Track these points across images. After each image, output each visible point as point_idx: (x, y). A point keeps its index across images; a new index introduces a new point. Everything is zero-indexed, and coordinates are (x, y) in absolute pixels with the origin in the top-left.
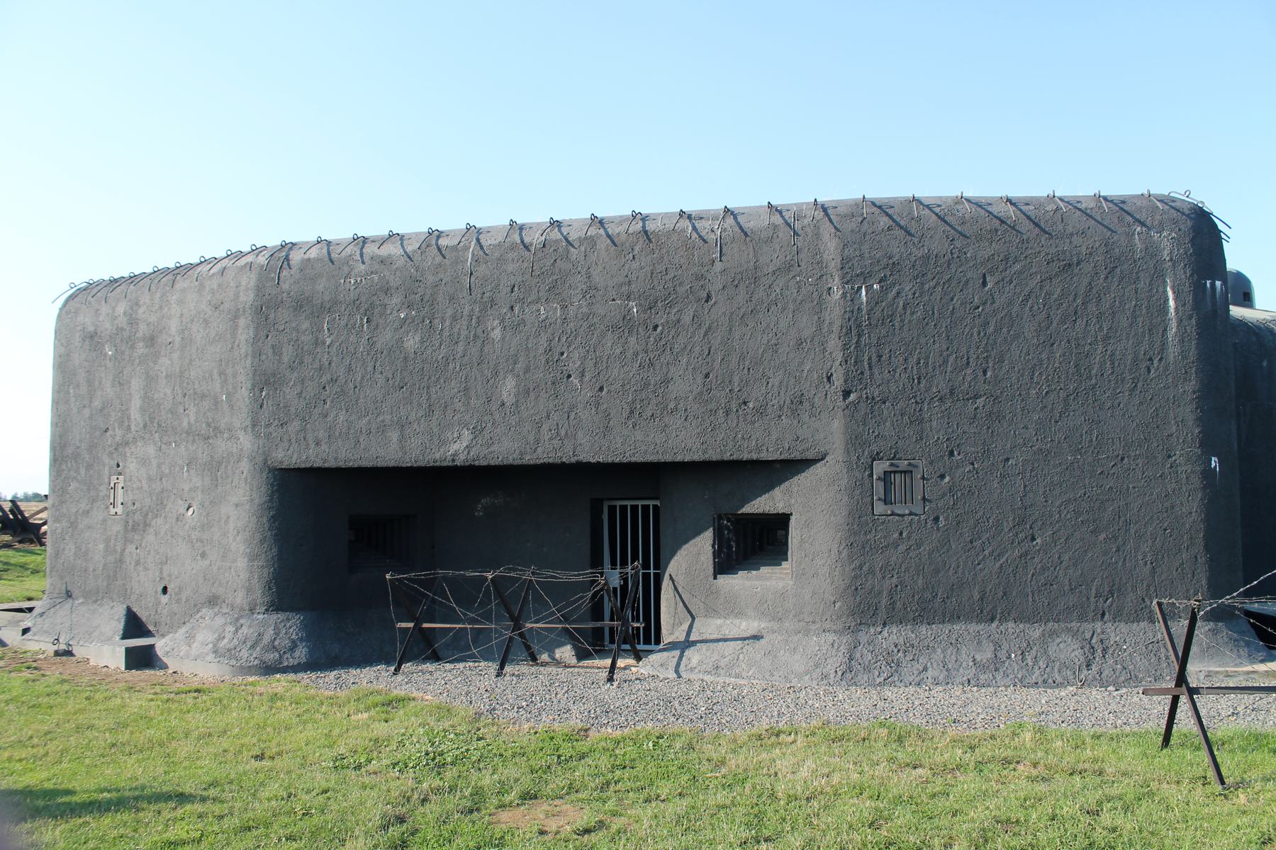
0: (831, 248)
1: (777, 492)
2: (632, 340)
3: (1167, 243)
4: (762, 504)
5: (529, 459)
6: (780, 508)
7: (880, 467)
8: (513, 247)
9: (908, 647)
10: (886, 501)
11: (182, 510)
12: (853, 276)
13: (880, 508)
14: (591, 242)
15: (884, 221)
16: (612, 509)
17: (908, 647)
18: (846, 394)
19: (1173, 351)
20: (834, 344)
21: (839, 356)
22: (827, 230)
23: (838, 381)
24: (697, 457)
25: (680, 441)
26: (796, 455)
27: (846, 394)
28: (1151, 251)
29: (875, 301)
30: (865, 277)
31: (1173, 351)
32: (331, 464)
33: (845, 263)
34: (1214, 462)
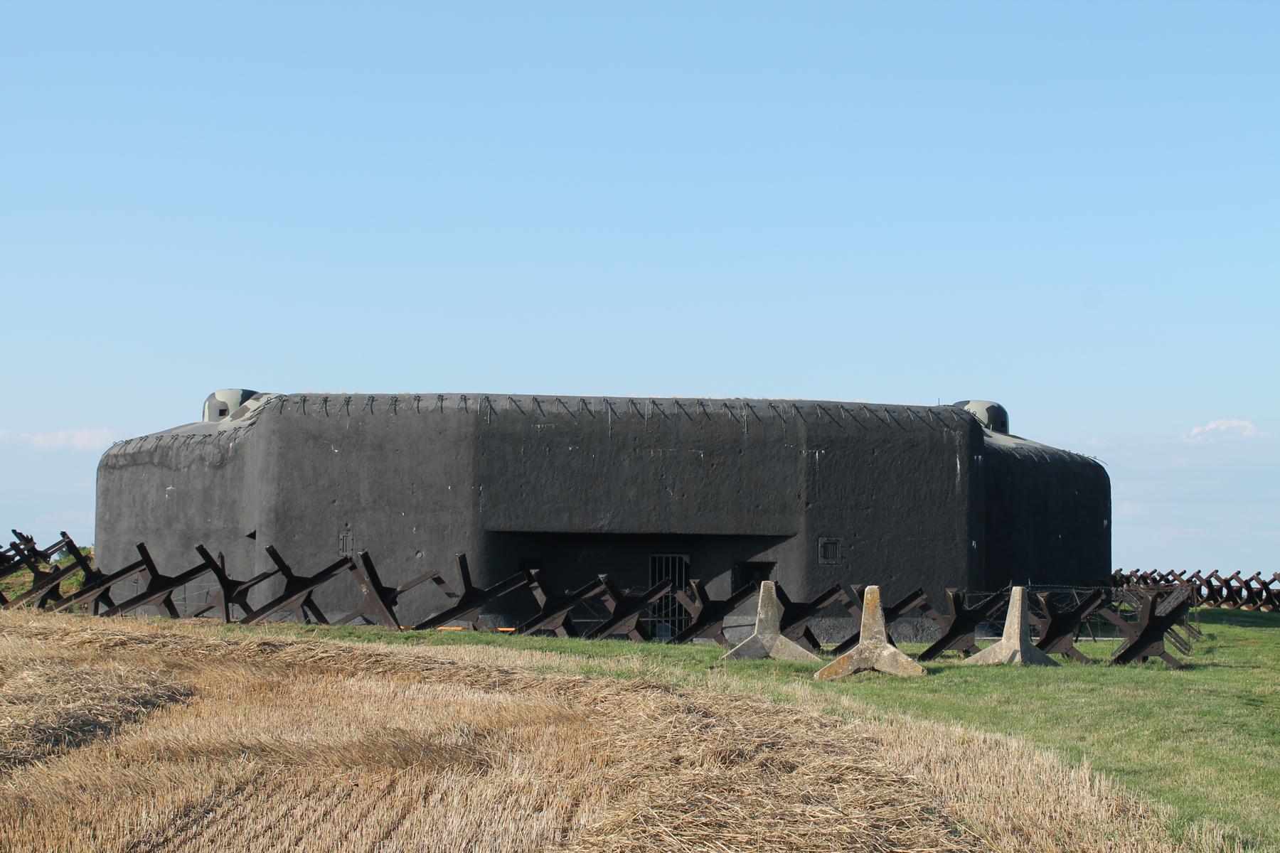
0: (802, 432)
1: (770, 551)
2: (701, 471)
3: (958, 436)
4: (760, 557)
5: (644, 530)
6: (771, 559)
7: (821, 541)
8: (633, 416)
9: (835, 627)
10: (825, 557)
11: (412, 554)
12: (812, 444)
13: (821, 561)
14: (678, 416)
15: (827, 419)
16: (654, 559)
17: (835, 627)
18: (807, 504)
19: (958, 489)
20: (802, 479)
21: (805, 485)
22: (800, 421)
23: (804, 498)
24: (733, 532)
25: (728, 525)
26: (782, 533)
27: (807, 504)
28: (951, 440)
29: (822, 457)
30: (818, 447)
31: (958, 489)
32: (526, 529)
33: (809, 440)
34: (974, 543)
